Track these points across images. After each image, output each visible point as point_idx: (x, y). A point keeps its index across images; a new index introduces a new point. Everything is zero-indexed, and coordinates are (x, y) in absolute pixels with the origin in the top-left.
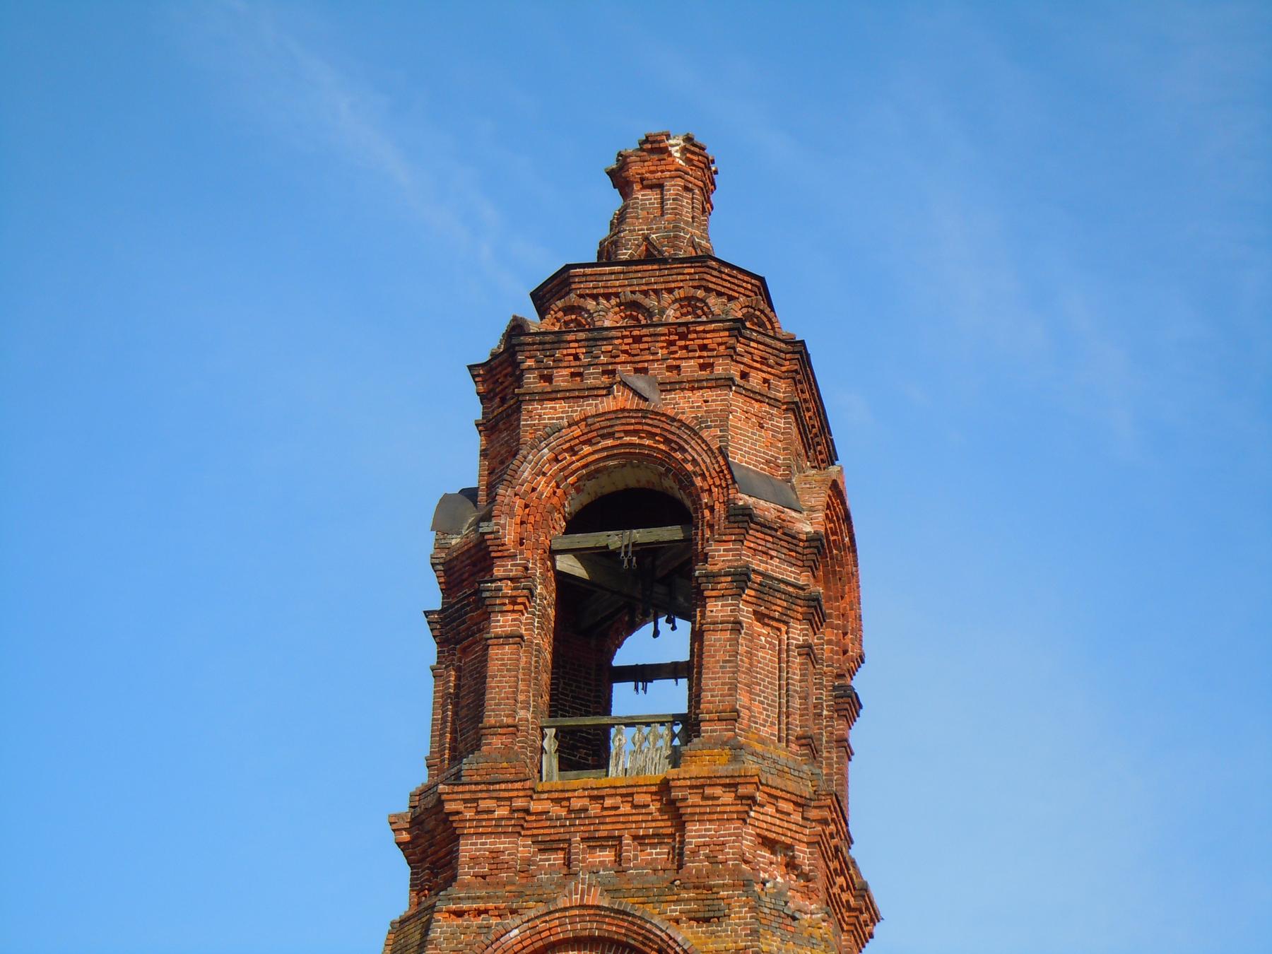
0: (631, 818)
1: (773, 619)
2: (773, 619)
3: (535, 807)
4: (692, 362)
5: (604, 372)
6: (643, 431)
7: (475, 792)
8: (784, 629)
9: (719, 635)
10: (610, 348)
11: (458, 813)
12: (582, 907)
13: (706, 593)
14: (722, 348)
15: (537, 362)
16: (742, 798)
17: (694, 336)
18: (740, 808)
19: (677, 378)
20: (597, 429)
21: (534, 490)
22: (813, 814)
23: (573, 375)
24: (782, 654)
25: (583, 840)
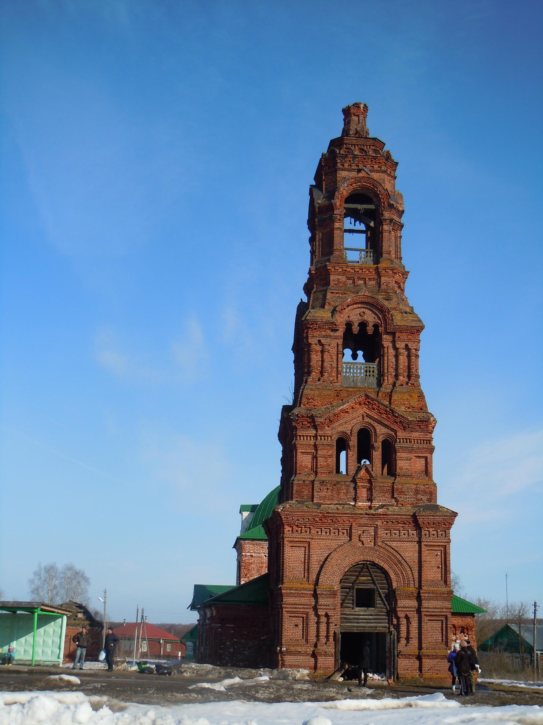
3: (348, 270)
4: (376, 166)
5: (356, 165)
9: (386, 234)
10: (358, 160)
11: (330, 269)
12: (364, 295)
13: (383, 223)
14: (384, 163)
15: (341, 161)
16: (394, 273)
17: (377, 160)
18: (393, 275)
19: (373, 169)
20: (357, 180)
21: (343, 193)
23: (349, 165)
25: (357, 278)
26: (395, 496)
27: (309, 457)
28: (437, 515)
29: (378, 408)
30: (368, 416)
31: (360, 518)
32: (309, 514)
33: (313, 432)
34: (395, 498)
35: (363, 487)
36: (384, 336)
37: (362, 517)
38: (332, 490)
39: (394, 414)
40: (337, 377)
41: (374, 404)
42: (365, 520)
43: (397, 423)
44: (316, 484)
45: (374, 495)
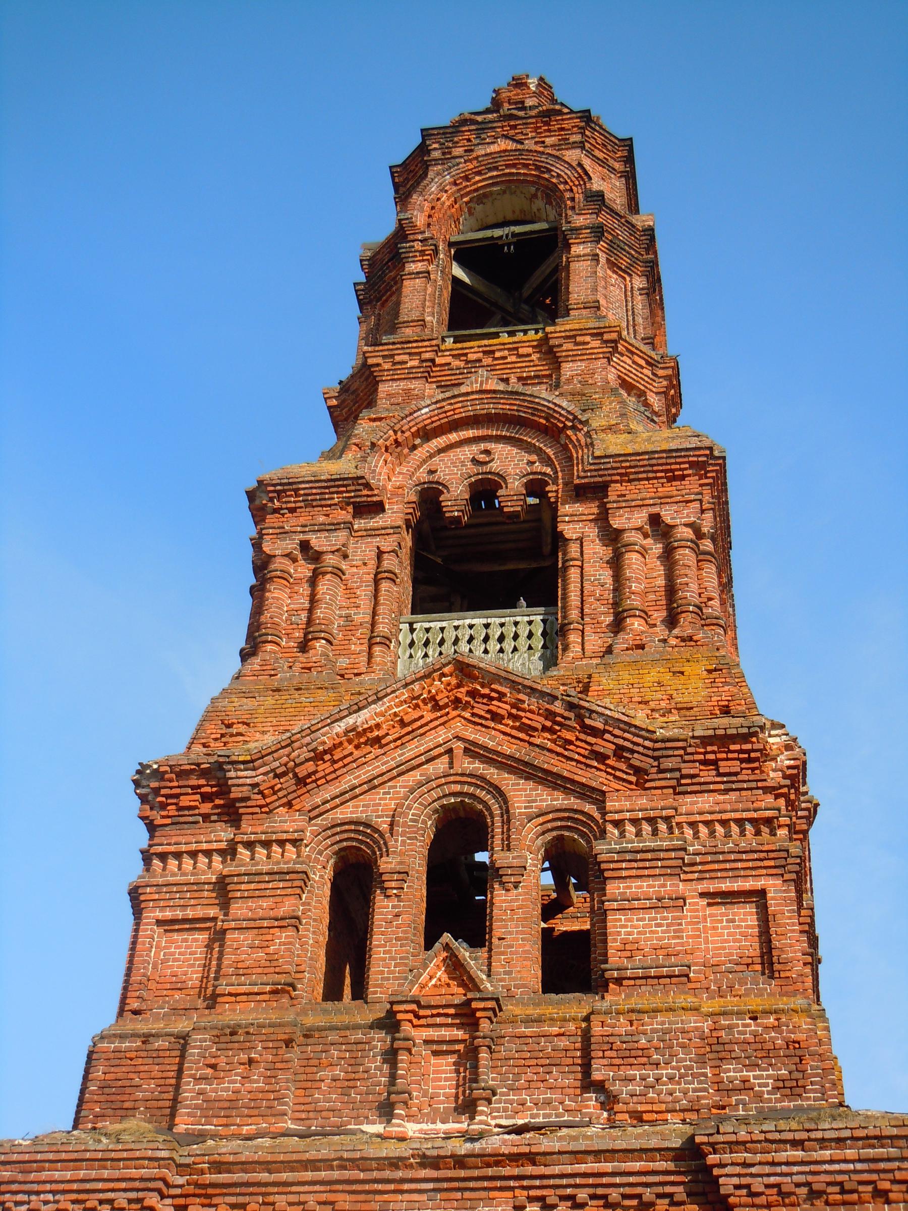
0: (517, 365)
1: (620, 269)
2: (620, 269)
6: (520, 164)
7: (392, 350)
8: (628, 279)
11: (378, 365)
16: (607, 342)
22: (661, 373)
24: (628, 294)
26: (597, 1076)
27: (196, 940)
28: (819, 1135)
29: (514, 711)
30: (473, 750)
31: (392, 1187)
32: (116, 1174)
33: (223, 833)
34: (599, 1087)
35: (438, 1048)
36: (566, 509)
37: (403, 1181)
38: (272, 1067)
39: (588, 721)
40: (370, 656)
41: (494, 695)
42: (415, 1197)
43: (601, 758)
44: (199, 1045)
45: (489, 1078)
